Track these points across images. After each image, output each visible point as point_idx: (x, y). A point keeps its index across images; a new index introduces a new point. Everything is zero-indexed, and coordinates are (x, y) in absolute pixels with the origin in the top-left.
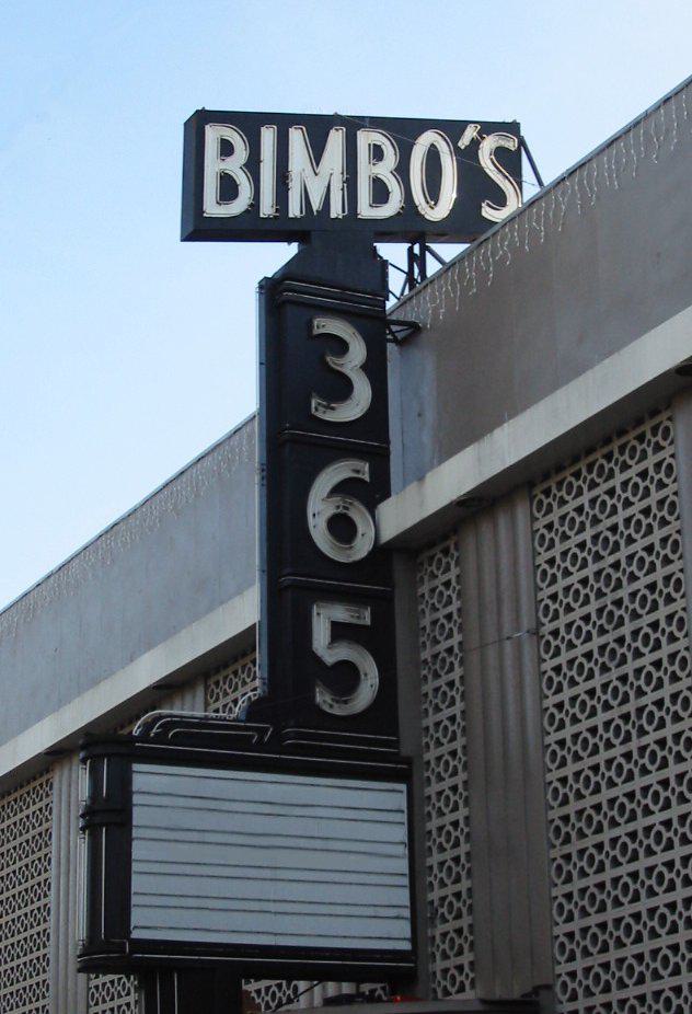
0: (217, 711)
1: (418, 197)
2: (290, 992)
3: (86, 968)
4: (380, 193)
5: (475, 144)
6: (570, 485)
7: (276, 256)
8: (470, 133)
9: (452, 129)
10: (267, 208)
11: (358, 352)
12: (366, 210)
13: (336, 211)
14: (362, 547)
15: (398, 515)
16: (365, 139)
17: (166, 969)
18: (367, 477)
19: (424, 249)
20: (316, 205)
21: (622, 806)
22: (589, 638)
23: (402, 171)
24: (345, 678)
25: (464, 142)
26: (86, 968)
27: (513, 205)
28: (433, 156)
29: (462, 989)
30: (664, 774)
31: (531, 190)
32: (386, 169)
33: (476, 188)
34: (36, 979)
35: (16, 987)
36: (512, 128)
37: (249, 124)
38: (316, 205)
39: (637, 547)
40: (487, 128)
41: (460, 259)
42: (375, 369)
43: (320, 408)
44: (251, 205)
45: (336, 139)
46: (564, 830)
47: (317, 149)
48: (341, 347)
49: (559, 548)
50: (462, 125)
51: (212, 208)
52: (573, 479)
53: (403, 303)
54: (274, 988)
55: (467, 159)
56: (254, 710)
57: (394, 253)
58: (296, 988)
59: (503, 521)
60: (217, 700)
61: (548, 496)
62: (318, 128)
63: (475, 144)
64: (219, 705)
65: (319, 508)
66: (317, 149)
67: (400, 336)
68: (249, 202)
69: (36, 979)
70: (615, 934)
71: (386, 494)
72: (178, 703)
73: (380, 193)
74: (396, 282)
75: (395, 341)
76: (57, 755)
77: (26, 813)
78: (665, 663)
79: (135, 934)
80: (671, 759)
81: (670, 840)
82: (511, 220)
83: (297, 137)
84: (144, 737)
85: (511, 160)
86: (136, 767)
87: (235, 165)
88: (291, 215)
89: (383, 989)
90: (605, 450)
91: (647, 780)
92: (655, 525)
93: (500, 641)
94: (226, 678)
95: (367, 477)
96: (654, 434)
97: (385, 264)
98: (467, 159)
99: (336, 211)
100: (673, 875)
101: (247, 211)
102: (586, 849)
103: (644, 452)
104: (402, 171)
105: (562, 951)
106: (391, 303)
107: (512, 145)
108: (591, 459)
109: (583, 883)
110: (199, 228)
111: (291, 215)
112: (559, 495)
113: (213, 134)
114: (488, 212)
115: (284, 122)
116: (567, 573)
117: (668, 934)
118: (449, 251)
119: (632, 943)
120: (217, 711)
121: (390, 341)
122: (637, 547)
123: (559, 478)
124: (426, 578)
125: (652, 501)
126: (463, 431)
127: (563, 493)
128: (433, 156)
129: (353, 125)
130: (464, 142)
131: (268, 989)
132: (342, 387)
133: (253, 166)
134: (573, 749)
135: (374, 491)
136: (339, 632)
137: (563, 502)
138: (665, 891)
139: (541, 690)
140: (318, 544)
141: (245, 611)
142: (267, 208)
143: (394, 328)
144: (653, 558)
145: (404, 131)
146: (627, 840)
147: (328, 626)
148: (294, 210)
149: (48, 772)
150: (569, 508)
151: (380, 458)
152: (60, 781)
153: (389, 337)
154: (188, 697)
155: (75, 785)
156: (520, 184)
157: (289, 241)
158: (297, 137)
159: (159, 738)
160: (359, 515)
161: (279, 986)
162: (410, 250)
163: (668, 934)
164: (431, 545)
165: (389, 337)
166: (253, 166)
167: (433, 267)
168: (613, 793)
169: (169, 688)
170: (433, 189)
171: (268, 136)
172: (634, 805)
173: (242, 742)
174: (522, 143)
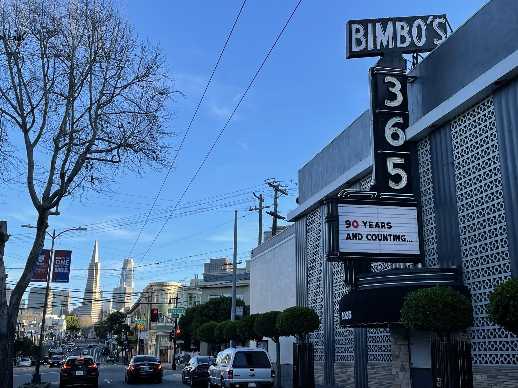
0: (363, 189)
1: (415, 40)
2: (386, 266)
3: (329, 260)
4: (404, 39)
5: (432, 22)
6: (472, 114)
7: (374, 60)
8: (430, 19)
9: (424, 18)
10: (370, 47)
11: (398, 86)
12: (399, 45)
13: (391, 46)
14: (400, 142)
15: (412, 132)
16: (399, 24)
17: (350, 260)
18: (402, 122)
19: (417, 55)
20: (385, 45)
21: (491, 209)
22: (469, 164)
23: (410, 32)
24: (397, 178)
25: (428, 22)
26: (329, 260)
27: (444, 39)
28: (419, 27)
29: (435, 265)
30: (482, 207)
31: (449, 34)
32: (405, 32)
33: (432, 35)
34: (318, 262)
35: (313, 264)
36: (443, 16)
37: (364, 23)
38: (385, 45)
39: (483, 137)
40: (435, 17)
41: (429, 57)
42: (404, 91)
43: (388, 103)
44: (366, 47)
45: (390, 25)
46: (463, 219)
47: (384, 29)
48: (393, 85)
49: (459, 138)
50: (428, 17)
51: (355, 49)
52: (463, 118)
53: (411, 71)
54: (382, 264)
55: (429, 27)
56: (372, 188)
57: (408, 57)
58: (388, 264)
59: (301, 220)
60: (363, 186)
61: (426, 143)
62: (384, 22)
63: (432, 22)
64: (364, 187)
65: (389, 131)
66: (384, 29)
67: (411, 81)
68: (365, 46)
69: (318, 262)
70: (480, 249)
71: (408, 126)
72: (352, 187)
73: (404, 39)
74: (409, 65)
75: (410, 82)
76: (320, 203)
77: (314, 218)
78: (463, 184)
79: (341, 251)
80: (495, 198)
81: (485, 225)
82: (442, 45)
83: (378, 26)
84: (341, 197)
85: (443, 26)
86: (339, 205)
87: (361, 35)
88: (377, 48)
89: (412, 265)
90: (473, 109)
91: (478, 208)
92: (460, 146)
93: (443, 166)
94: (365, 180)
95: (402, 122)
96: (468, 115)
97: (405, 60)
98: (429, 27)
99: (391, 46)
100: (476, 239)
101: (365, 48)
102: (470, 225)
103: (485, 109)
104: (410, 32)
105: (505, 242)
106: (408, 72)
107: (443, 21)
108: (478, 106)
109: (479, 231)
110: (352, 55)
111: (377, 48)
112: (459, 123)
113: (354, 27)
114: (436, 42)
115: (374, 22)
116: (471, 140)
117: (496, 249)
118: (425, 55)
119: (485, 252)
120: (363, 189)
121: (408, 82)
122: (483, 137)
123: (487, 100)
124: (420, 149)
125: (487, 123)
126: (427, 108)
127: (479, 110)
128: (419, 27)
129: (394, 20)
130: (428, 22)
131: (380, 264)
132: (393, 97)
133: (366, 35)
134: (465, 196)
135: (404, 126)
136: (395, 165)
137: (460, 125)
138: (484, 240)
139: (455, 179)
140: (388, 140)
141: (369, 161)
142: (370, 47)
143: (409, 78)
144: (459, 155)
145: (410, 21)
146: (482, 222)
147: (392, 164)
148: (378, 47)
149: (319, 207)
150: (462, 127)
151: (406, 117)
152: (322, 209)
153: (408, 81)
154: (355, 186)
155: (325, 210)
156: (446, 32)
157: (377, 56)
158: (378, 26)
159: (346, 197)
160: (400, 132)
161: (383, 264)
162: (413, 55)
163: (496, 249)
164: (422, 140)
165: (408, 81)
166: (366, 35)
167: (420, 60)
168: (478, 208)
169: (350, 183)
170: (420, 38)
171: (370, 26)
172: (484, 212)
173: (369, 197)
174: (446, 20)
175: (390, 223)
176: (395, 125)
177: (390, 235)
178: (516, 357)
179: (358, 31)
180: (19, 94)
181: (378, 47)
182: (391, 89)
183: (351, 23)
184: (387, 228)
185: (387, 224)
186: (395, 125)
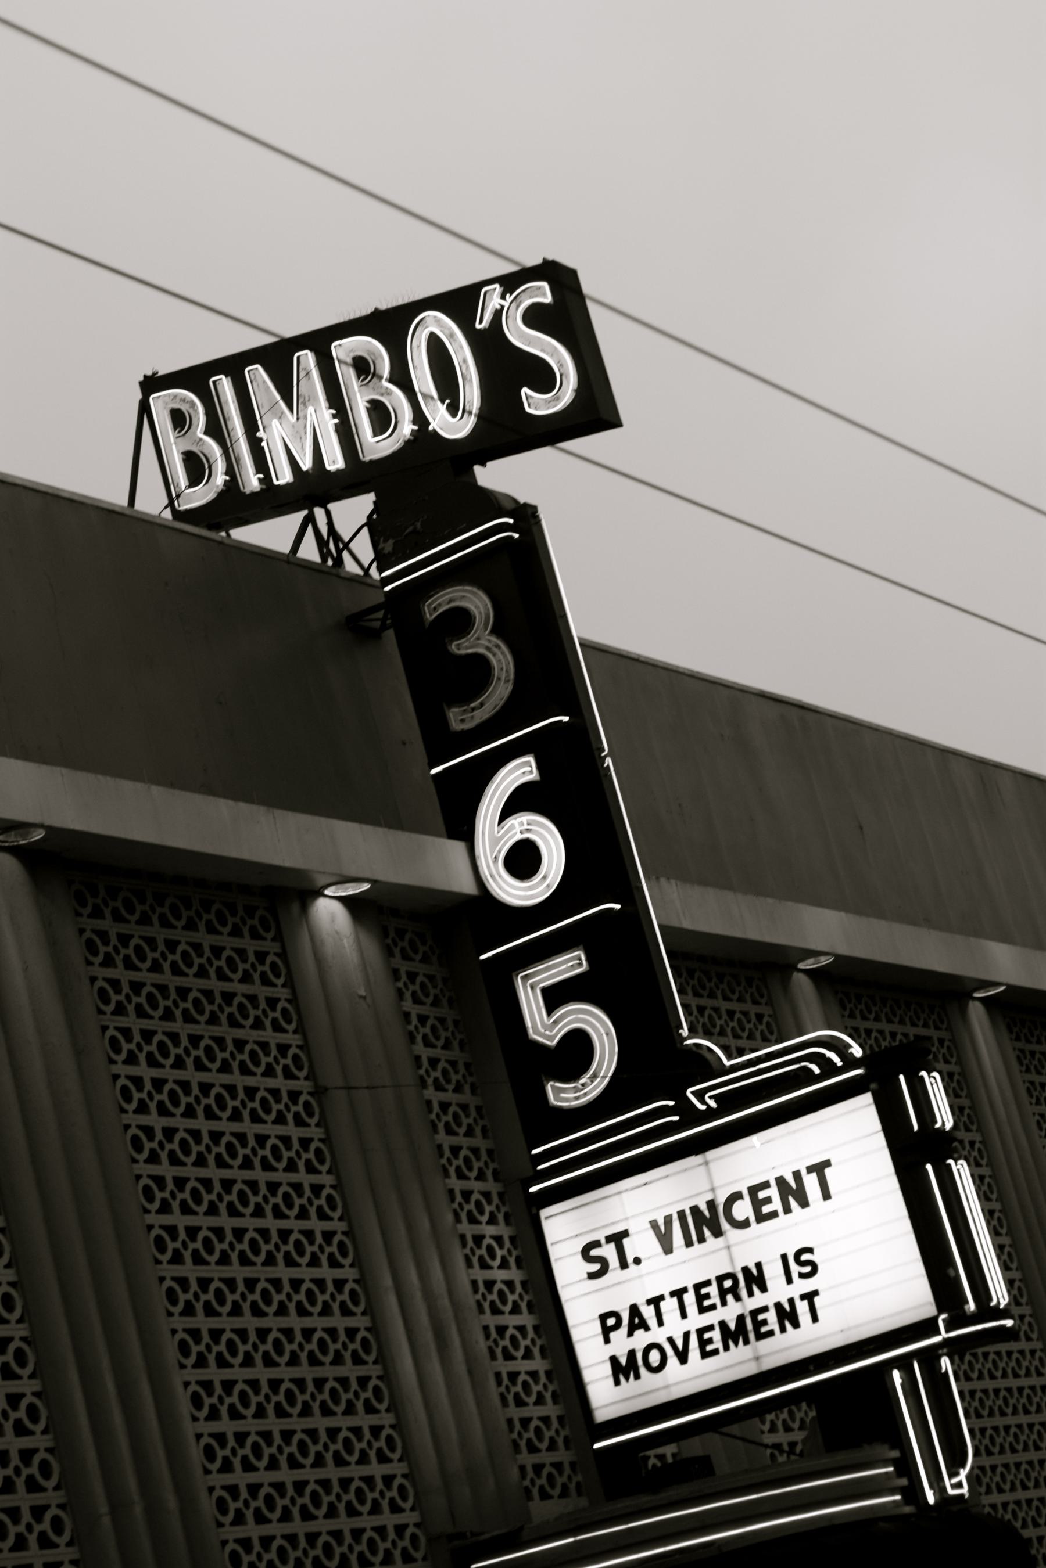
16: (343, 349)
20: (306, 463)
38: (306, 463)
133: (216, 429)
142: (252, 482)
158: (257, 375)
166: (216, 429)
171: (225, 385)
175: (810, 1250)
176: (512, 806)
177: (656, 1302)
178: (11, 1540)
179: (179, 420)
180: (564, 966)
181: (284, 476)
182: (461, 647)
183: (151, 384)
184: (802, 1276)
185: (798, 1254)
186: (512, 806)
